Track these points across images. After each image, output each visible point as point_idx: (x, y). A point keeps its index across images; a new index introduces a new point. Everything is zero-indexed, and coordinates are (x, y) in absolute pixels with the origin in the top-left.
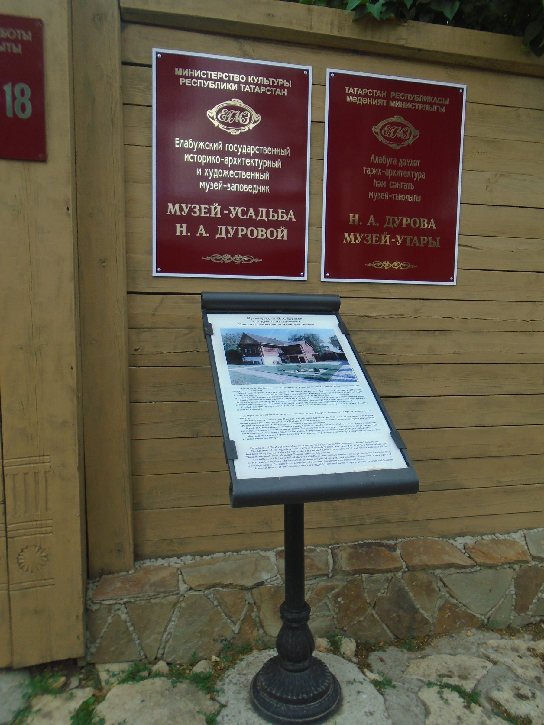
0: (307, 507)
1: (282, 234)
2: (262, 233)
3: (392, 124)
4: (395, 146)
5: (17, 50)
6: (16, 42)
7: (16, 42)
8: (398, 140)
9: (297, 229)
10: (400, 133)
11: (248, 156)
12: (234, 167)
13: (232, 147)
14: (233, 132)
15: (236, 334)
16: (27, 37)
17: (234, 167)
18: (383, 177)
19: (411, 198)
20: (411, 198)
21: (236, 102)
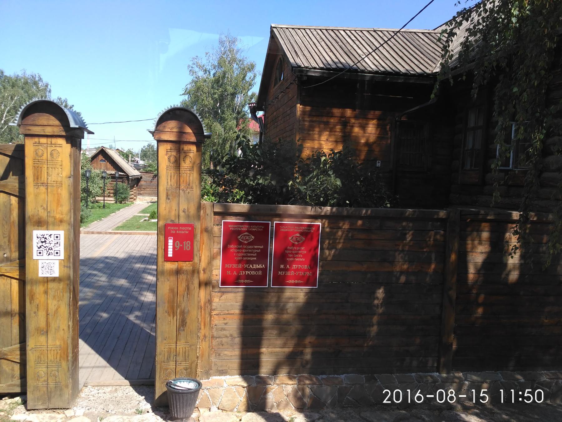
0: (84, 254)
1: (260, 273)
2: (253, 273)
3: (245, 235)
4: (246, 242)
5: (187, 232)
6: (187, 230)
7: (187, 230)
8: (247, 240)
9: (264, 270)
10: (247, 238)
11: (250, 249)
12: (245, 253)
13: (245, 247)
14: (246, 242)
15: (266, 312)
16: (190, 229)
17: (245, 253)
18: (292, 253)
19: (301, 260)
20: (301, 260)
21: (246, 233)
